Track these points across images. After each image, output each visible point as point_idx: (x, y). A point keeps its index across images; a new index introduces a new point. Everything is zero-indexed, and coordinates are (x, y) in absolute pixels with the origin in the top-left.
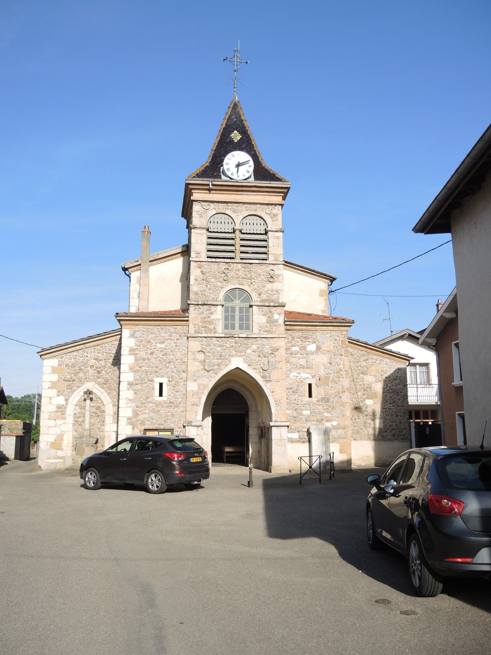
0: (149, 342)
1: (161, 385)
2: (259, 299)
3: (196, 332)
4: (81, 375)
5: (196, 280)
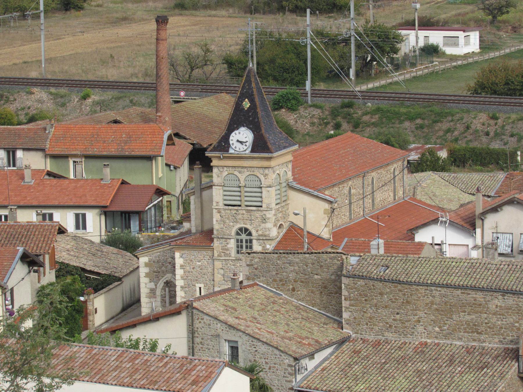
0: (191, 261)
1: (200, 288)
2: (257, 234)
3: (218, 256)
4: (163, 268)
5: (217, 221)
